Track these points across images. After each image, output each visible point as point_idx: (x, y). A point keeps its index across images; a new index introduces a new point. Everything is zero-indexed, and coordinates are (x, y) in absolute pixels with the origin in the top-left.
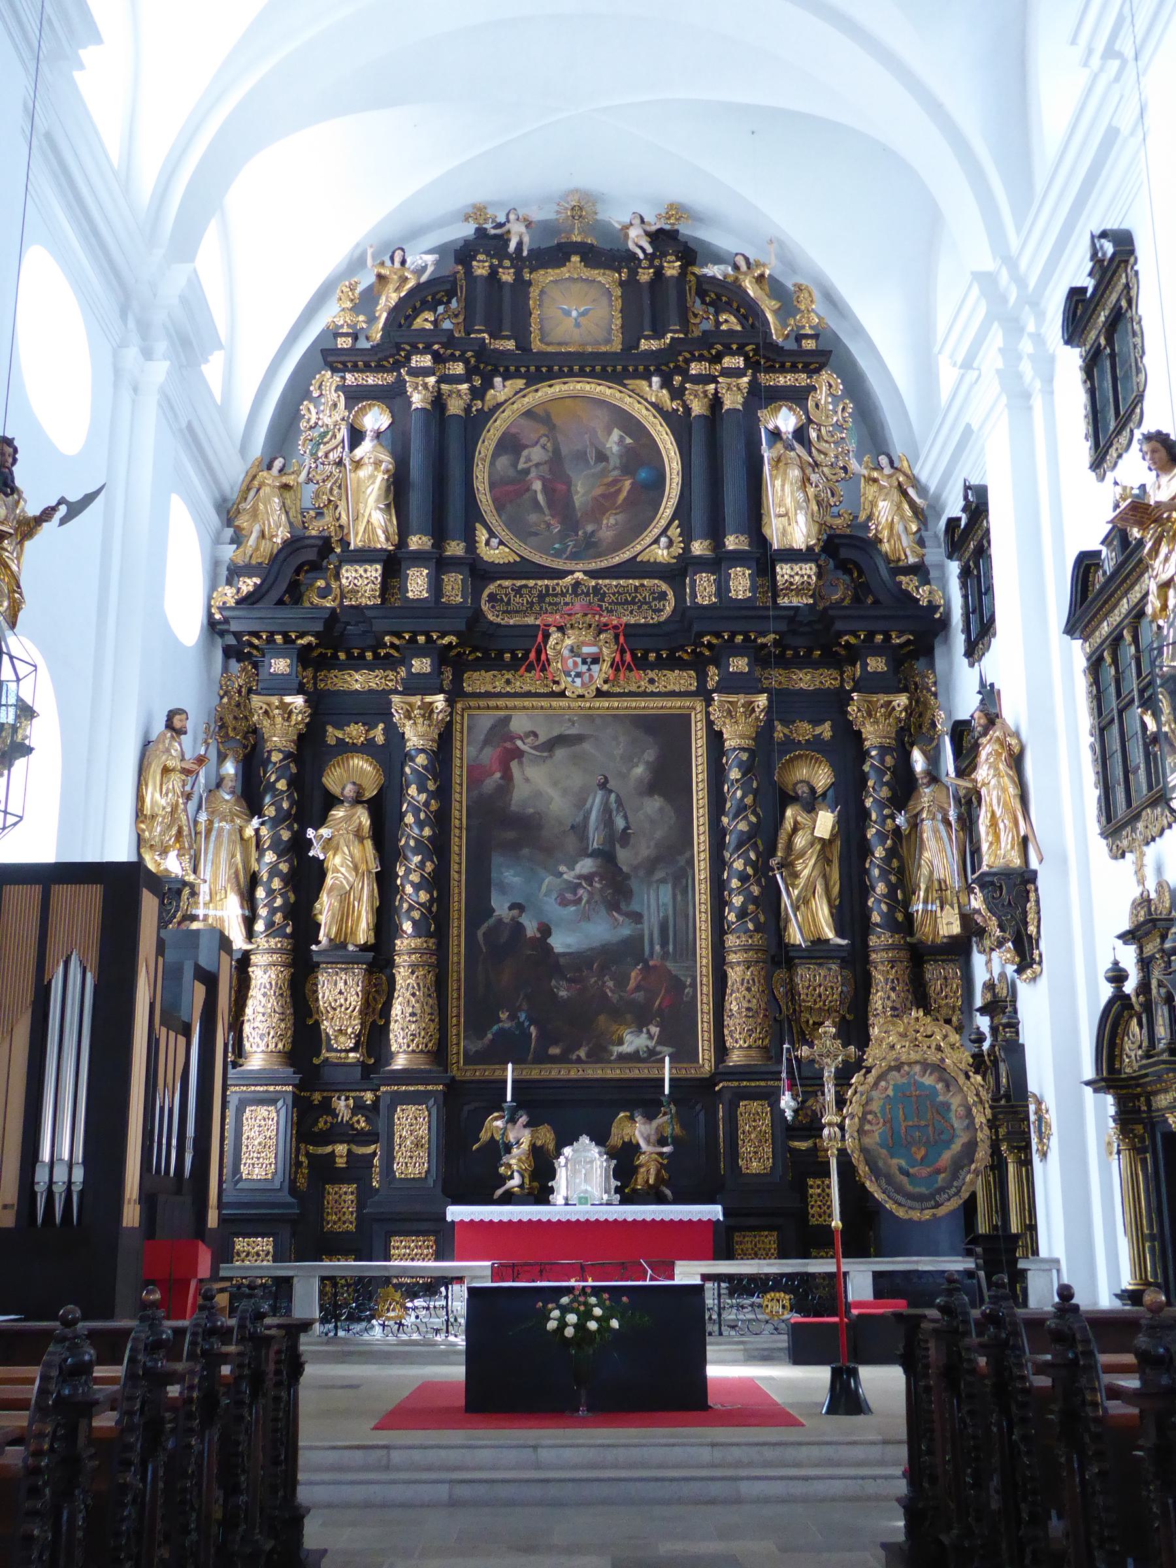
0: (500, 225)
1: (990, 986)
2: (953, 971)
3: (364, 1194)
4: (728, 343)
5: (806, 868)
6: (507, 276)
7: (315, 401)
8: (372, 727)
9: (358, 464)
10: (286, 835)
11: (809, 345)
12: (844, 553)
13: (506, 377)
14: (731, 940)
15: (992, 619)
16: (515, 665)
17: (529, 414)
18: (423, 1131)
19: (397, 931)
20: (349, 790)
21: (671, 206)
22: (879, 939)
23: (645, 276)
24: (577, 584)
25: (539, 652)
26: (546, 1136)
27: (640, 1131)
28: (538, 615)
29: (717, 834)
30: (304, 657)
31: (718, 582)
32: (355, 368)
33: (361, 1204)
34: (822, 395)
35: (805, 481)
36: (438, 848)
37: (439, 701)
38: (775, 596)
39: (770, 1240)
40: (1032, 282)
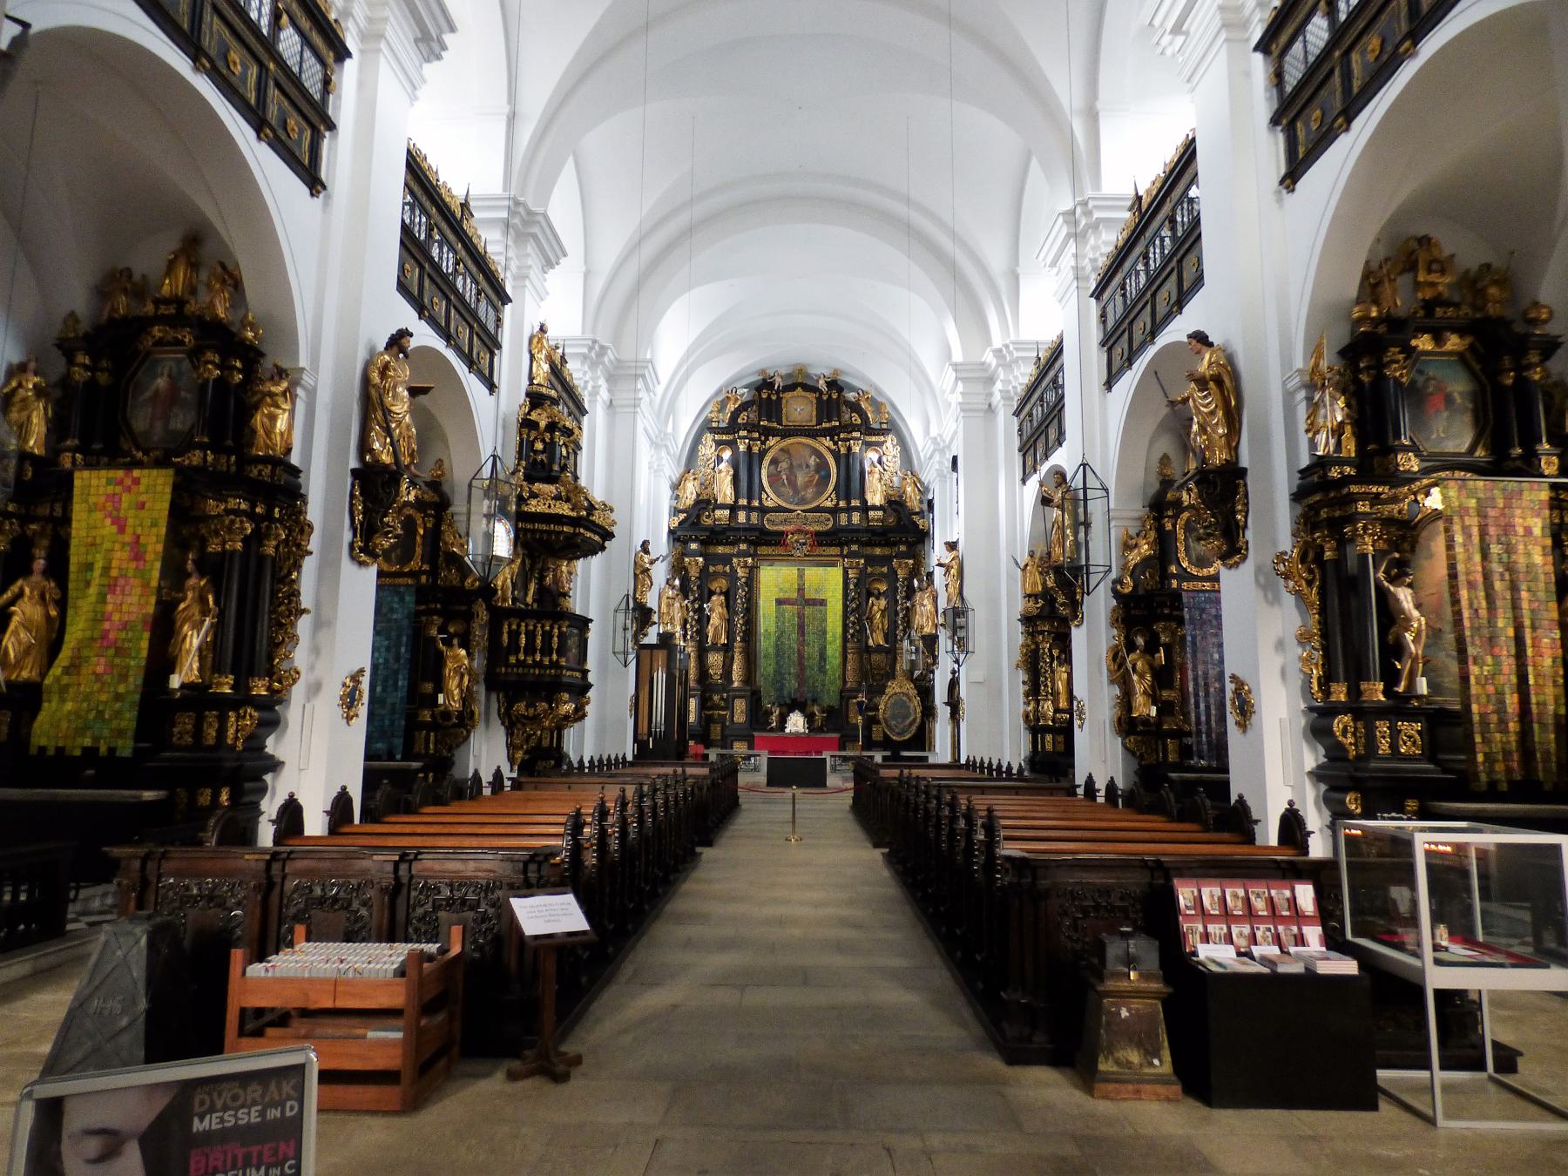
3: (724, 727)
4: (854, 428)
6: (774, 398)
8: (725, 566)
9: (720, 472)
11: (884, 426)
14: (849, 645)
17: (782, 450)
19: (735, 640)
23: (825, 397)
30: (703, 543)
33: (722, 730)
34: (889, 444)
35: (880, 479)
37: (750, 560)
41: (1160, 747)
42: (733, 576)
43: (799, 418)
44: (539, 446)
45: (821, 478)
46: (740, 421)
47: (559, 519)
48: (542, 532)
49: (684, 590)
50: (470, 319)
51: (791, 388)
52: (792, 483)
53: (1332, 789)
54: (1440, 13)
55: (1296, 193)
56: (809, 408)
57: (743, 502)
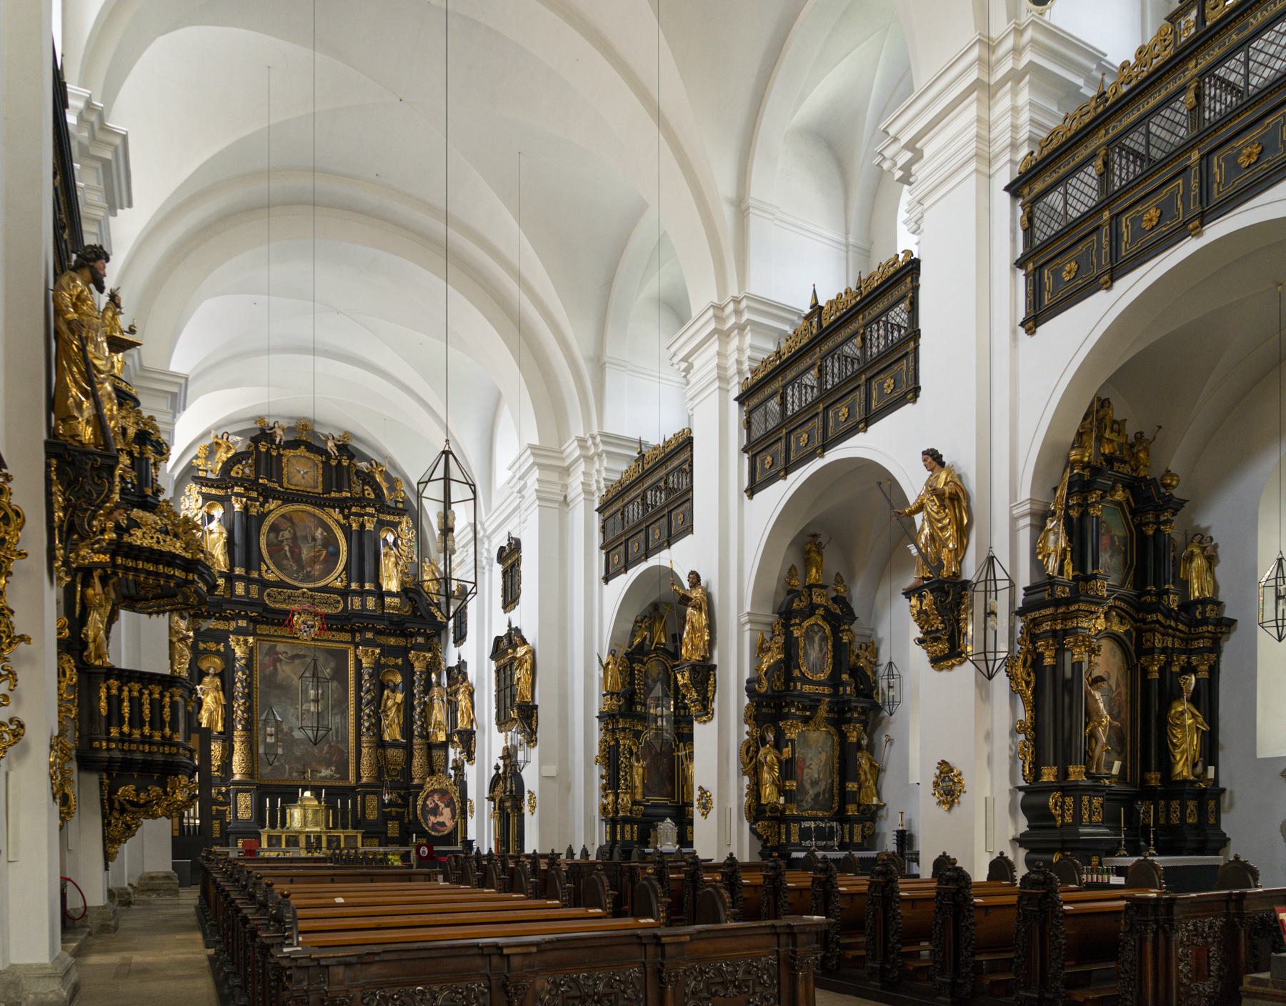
0: (272, 429)
1: (455, 761)
2: (442, 753)
4: (369, 503)
5: (392, 713)
6: (274, 453)
7: (188, 497)
8: (219, 644)
11: (400, 506)
12: (411, 595)
13: (274, 498)
14: (364, 739)
15: (465, 635)
17: (283, 516)
18: (249, 803)
19: (233, 728)
20: (212, 671)
21: (346, 433)
22: (417, 741)
23: (334, 463)
24: (304, 593)
25: (290, 621)
28: (288, 604)
29: (359, 700)
31: (362, 601)
32: (206, 485)
34: (404, 525)
35: (397, 564)
36: (248, 696)
37: (251, 640)
38: (383, 609)
39: (376, 841)
40: (488, 532)
41: (783, 830)
42: (228, 657)
46: (233, 474)
47: (171, 559)
48: (149, 573)
51: (294, 444)
52: (296, 557)
53: (1032, 851)
54: (1243, 198)
55: (1035, 337)
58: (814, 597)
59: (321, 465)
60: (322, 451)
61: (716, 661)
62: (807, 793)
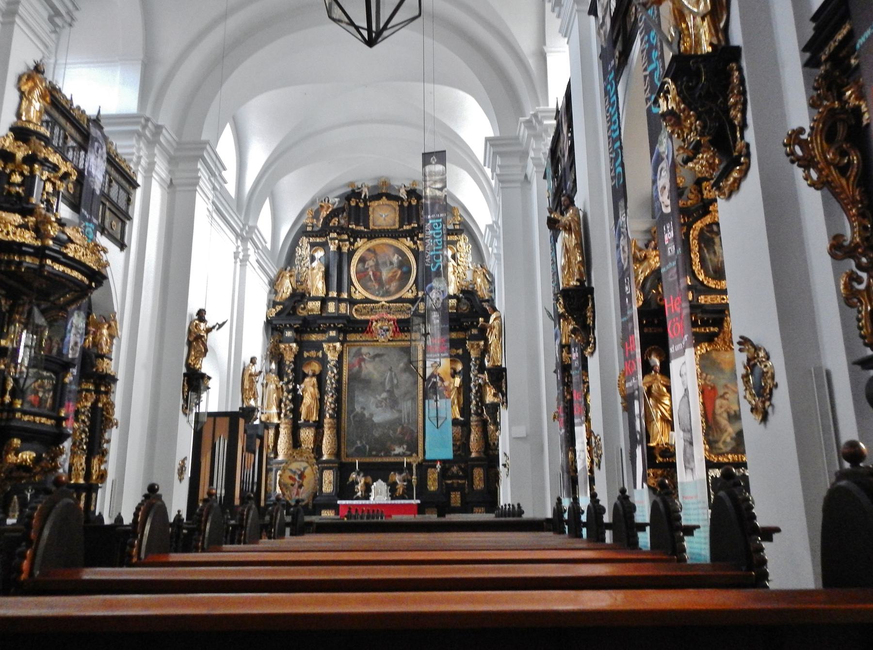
0: (359, 188)
6: (362, 205)
7: (301, 247)
8: (318, 351)
9: (313, 269)
10: (291, 387)
11: (457, 227)
16: (363, 332)
17: (369, 250)
19: (325, 417)
20: (310, 373)
21: (414, 181)
22: (474, 418)
23: (406, 204)
26: (369, 479)
27: (397, 478)
28: (370, 315)
30: (296, 331)
32: (313, 236)
34: (462, 243)
37: (338, 345)
42: (323, 361)
43: (384, 223)
44: (17, 178)
45: (403, 273)
47: (17, 248)
49: (280, 374)
50: (121, 217)
56: (392, 215)
57: (333, 294)
58: (705, 192)
59: (397, 208)
60: (397, 198)
61: (593, 285)
62: (722, 431)
